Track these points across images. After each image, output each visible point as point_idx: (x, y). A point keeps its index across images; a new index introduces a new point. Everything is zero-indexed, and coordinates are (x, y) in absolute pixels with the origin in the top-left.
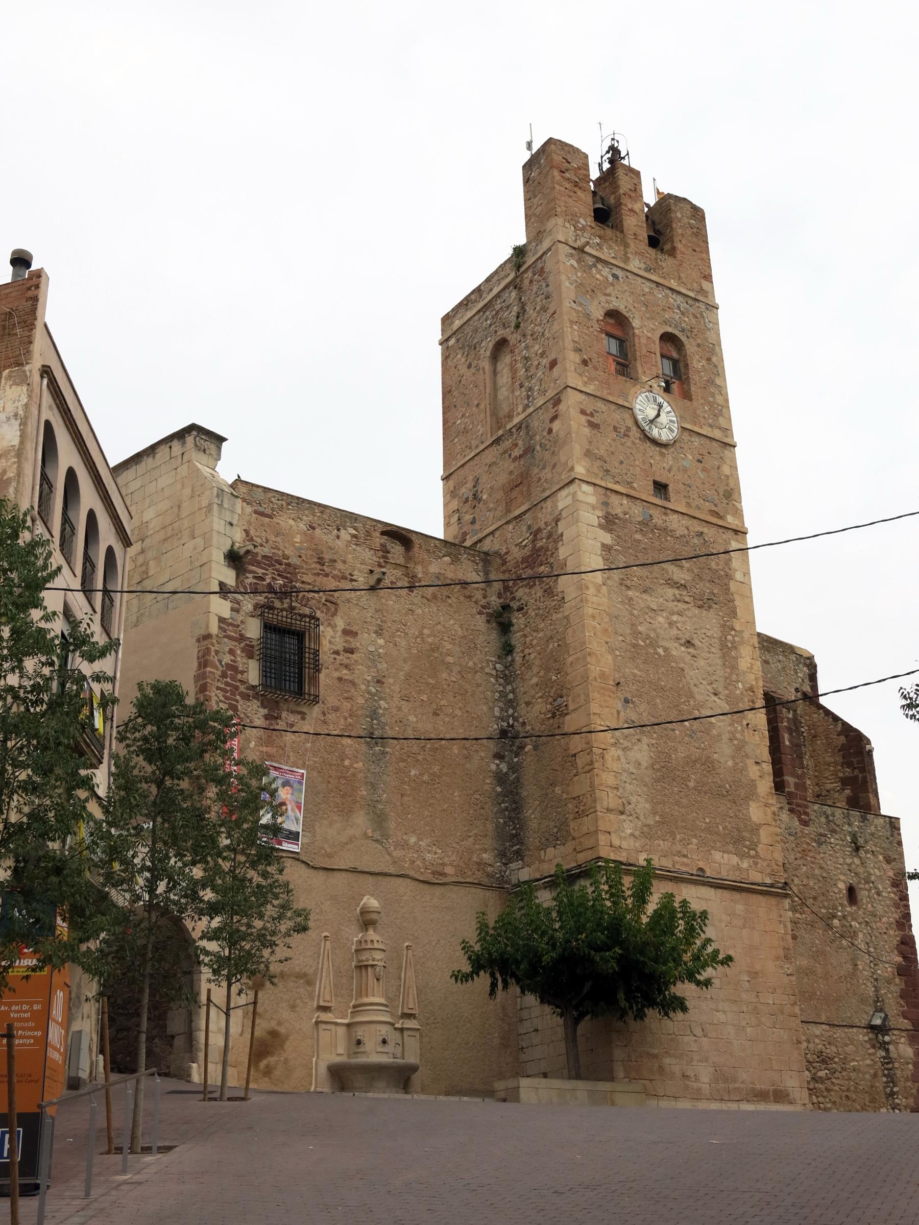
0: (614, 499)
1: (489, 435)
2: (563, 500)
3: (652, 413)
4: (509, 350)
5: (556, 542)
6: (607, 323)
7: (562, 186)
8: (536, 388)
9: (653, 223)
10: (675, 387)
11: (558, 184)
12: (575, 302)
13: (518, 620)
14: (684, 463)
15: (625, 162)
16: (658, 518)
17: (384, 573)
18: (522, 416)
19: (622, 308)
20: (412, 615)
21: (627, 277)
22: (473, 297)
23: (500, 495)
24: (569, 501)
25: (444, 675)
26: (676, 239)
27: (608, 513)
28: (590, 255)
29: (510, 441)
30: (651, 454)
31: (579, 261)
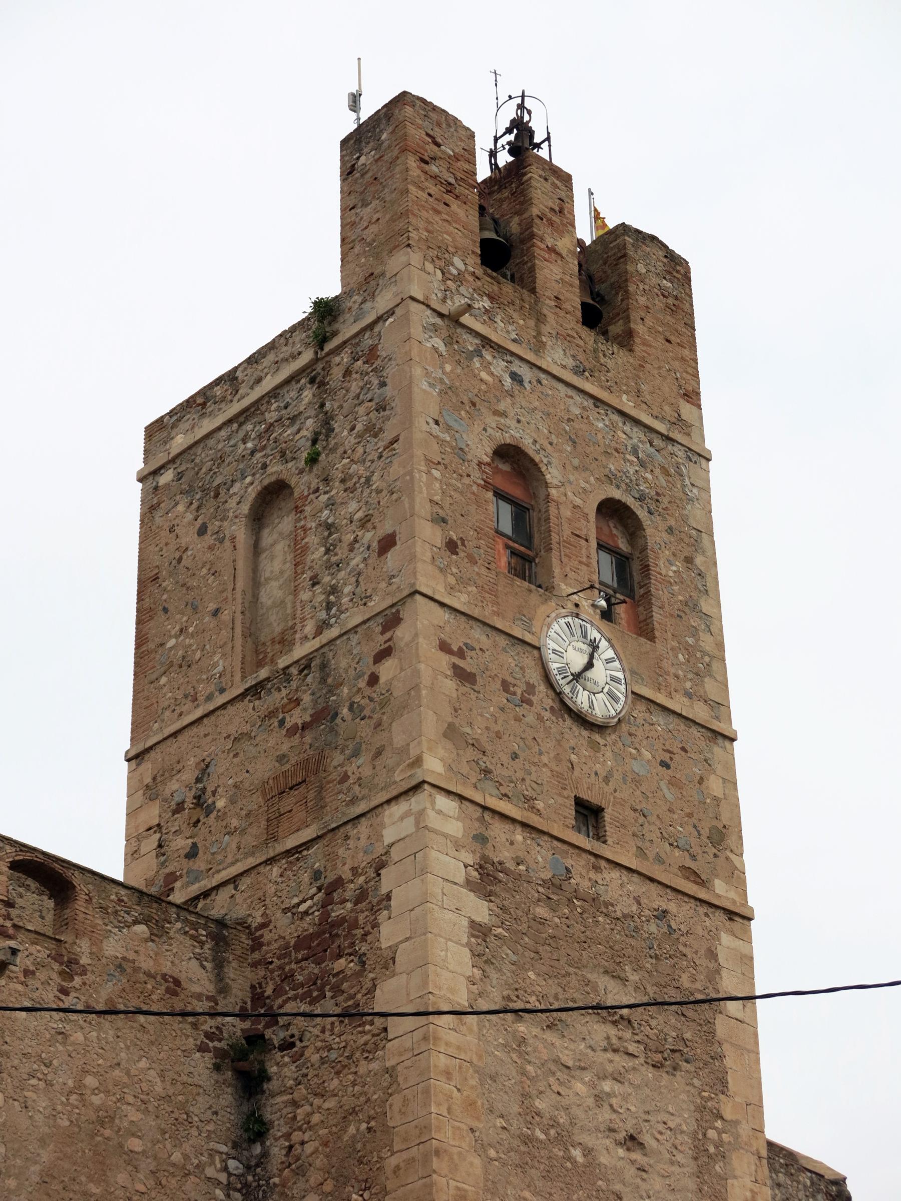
0: (498, 831)
1: (238, 677)
2: (395, 824)
3: (578, 661)
4: (291, 505)
5: (374, 910)
6: (497, 471)
7: (423, 190)
8: (347, 590)
9: (590, 278)
10: (621, 611)
11: (415, 184)
12: (437, 423)
13: (281, 1070)
14: (636, 766)
15: (543, 153)
16: (582, 877)
17: (14, 952)
18: (316, 643)
19: (527, 444)
20: (64, 1044)
21: (539, 382)
22: (218, 391)
23: (255, 802)
24: (408, 827)
25: (122, 1178)
26: (635, 315)
27: (484, 858)
28: (471, 331)
29: (284, 692)
30: (572, 743)
31: (449, 341)
